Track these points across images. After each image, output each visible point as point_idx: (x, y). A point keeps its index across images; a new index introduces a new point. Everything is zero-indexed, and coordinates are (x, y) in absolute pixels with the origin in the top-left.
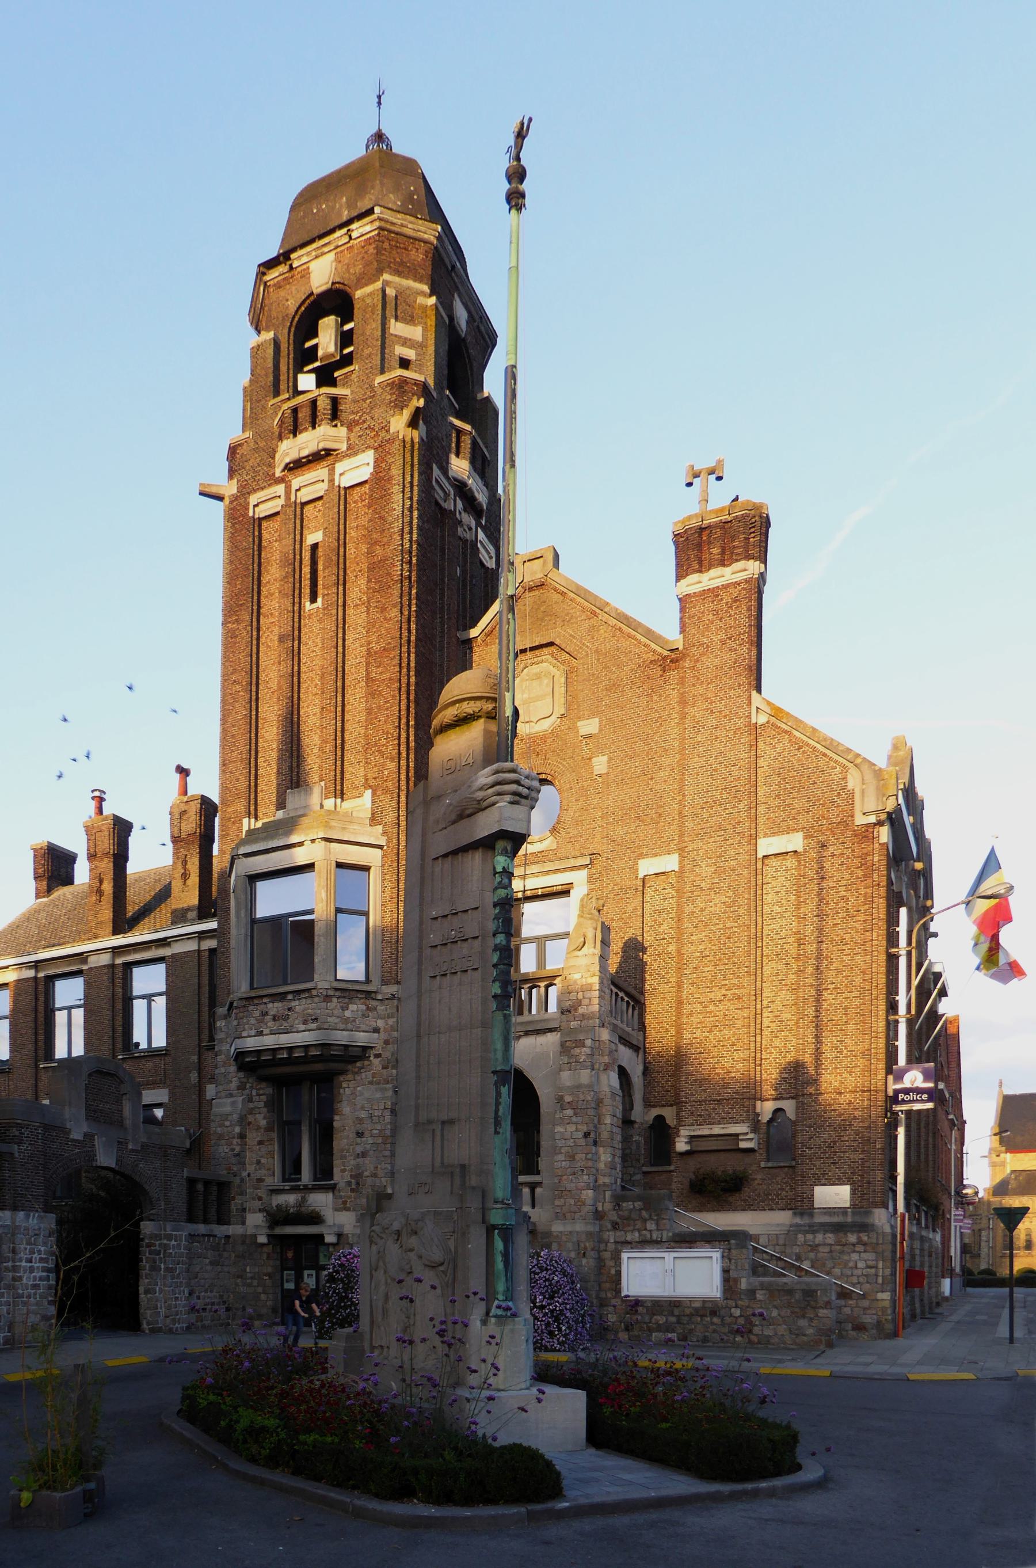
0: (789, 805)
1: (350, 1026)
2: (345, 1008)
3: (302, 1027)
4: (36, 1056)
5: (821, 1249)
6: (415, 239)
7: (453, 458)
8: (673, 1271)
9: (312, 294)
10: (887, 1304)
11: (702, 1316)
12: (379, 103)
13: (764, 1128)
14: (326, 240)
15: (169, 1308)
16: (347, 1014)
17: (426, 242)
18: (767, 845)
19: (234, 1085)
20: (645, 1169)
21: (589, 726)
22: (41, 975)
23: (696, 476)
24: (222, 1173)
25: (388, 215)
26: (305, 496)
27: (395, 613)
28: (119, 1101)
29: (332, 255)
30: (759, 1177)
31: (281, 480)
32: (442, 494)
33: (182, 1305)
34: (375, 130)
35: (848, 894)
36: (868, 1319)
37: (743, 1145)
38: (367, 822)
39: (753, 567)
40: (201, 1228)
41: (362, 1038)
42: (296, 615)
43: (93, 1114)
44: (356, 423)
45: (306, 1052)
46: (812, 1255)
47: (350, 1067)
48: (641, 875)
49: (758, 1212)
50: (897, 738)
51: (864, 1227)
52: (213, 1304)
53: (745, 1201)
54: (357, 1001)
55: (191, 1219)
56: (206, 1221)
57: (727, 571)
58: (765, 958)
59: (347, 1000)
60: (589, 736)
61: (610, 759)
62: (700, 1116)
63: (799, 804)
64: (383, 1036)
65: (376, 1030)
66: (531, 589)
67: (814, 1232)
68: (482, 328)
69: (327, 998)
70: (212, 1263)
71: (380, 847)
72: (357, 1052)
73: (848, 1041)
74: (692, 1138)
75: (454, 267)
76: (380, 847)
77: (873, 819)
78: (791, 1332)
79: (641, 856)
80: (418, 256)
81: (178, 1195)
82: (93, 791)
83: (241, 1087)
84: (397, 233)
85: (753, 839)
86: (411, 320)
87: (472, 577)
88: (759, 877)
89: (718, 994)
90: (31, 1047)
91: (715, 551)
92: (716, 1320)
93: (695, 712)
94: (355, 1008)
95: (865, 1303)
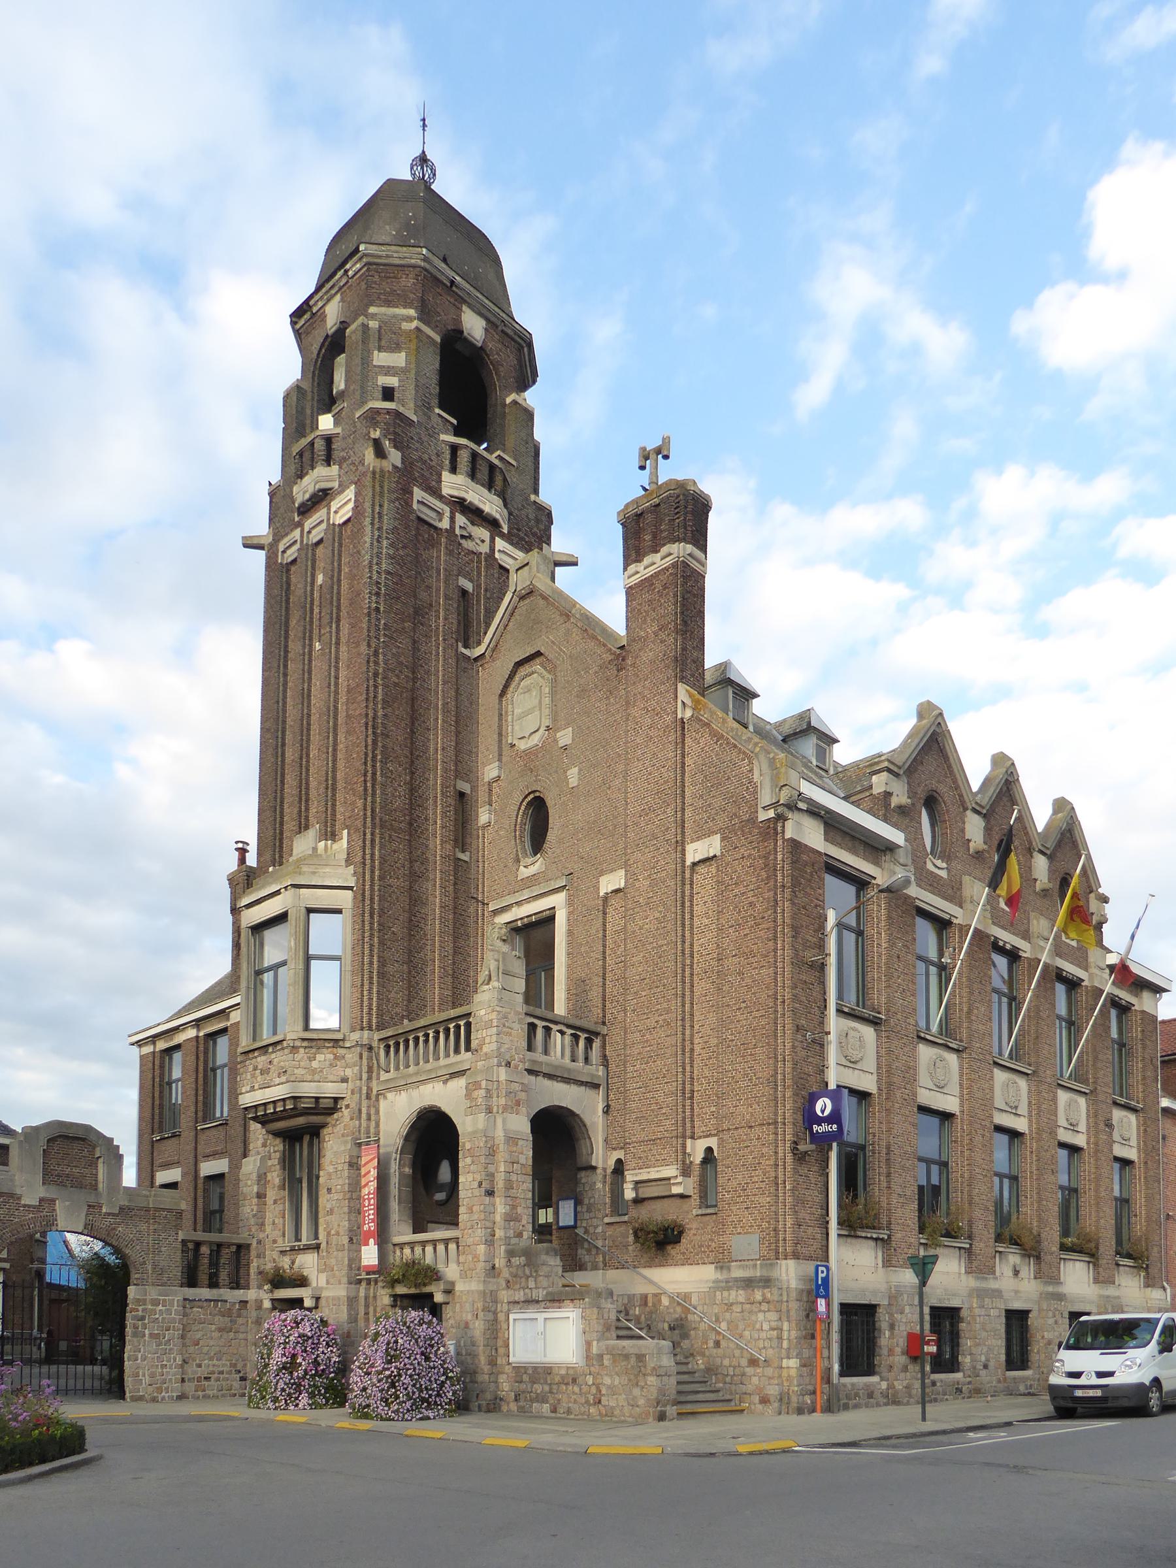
1: (317, 1077)
3: (277, 1081)
4: (196, 1118)
5: (734, 1307)
6: (403, 266)
7: (446, 476)
8: (544, 1333)
9: (327, 336)
10: (793, 1373)
11: (567, 1384)
12: (424, 125)
13: (696, 1171)
14: (331, 283)
15: (152, 1376)
17: (414, 267)
18: (696, 851)
19: (260, 1143)
20: (607, 1220)
21: (565, 737)
22: (201, 1034)
23: (647, 458)
24: (242, 1237)
25: (372, 250)
26: (315, 536)
27: (363, 648)
28: (93, 1163)
30: (694, 1226)
32: (433, 515)
33: (173, 1373)
34: (418, 153)
36: (773, 1391)
37: (676, 1190)
38: (343, 863)
39: (679, 550)
40: (204, 1293)
41: (330, 1089)
42: (307, 657)
43: (48, 1177)
44: (344, 459)
46: (727, 1315)
47: (329, 1119)
48: (601, 894)
49: (694, 1267)
50: (921, 706)
51: (767, 1282)
52: (222, 1373)
53: (684, 1254)
54: (325, 1050)
55: (191, 1280)
56: (213, 1284)
57: (656, 557)
58: (695, 977)
59: (314, 1050)
60: (565, 748)
61: (580, 770)
62: (640, 1158)
63: (718, 802)
64: (351, 1085)
65: (344, 1080)
66: (522, 598)
67: (729, 1289)
68: (509, 332)
69: (294, 1049)
70: (220, 1330)
71: (351, 888)
72: (328, 1104)
73: (757, 1067)
75: (452, 283)
76: (351, 888)
77: (771, 814)
78: (629, 1404)
79: (602, 873)
80: (408, 281)
81: (172, 1260)
82: (237, 842)
83: (264, 1145)
84: (385, 265)
85: (680, 846)
86: (395, 348)
87: (486, 590)
88: (687, 887)
89: (651, 1023)
90: (193, 1109)
91: (648, 537)
92: (576, 1389)
93: (635, 712)
94: (323, 1057)
95: (769, 1371)
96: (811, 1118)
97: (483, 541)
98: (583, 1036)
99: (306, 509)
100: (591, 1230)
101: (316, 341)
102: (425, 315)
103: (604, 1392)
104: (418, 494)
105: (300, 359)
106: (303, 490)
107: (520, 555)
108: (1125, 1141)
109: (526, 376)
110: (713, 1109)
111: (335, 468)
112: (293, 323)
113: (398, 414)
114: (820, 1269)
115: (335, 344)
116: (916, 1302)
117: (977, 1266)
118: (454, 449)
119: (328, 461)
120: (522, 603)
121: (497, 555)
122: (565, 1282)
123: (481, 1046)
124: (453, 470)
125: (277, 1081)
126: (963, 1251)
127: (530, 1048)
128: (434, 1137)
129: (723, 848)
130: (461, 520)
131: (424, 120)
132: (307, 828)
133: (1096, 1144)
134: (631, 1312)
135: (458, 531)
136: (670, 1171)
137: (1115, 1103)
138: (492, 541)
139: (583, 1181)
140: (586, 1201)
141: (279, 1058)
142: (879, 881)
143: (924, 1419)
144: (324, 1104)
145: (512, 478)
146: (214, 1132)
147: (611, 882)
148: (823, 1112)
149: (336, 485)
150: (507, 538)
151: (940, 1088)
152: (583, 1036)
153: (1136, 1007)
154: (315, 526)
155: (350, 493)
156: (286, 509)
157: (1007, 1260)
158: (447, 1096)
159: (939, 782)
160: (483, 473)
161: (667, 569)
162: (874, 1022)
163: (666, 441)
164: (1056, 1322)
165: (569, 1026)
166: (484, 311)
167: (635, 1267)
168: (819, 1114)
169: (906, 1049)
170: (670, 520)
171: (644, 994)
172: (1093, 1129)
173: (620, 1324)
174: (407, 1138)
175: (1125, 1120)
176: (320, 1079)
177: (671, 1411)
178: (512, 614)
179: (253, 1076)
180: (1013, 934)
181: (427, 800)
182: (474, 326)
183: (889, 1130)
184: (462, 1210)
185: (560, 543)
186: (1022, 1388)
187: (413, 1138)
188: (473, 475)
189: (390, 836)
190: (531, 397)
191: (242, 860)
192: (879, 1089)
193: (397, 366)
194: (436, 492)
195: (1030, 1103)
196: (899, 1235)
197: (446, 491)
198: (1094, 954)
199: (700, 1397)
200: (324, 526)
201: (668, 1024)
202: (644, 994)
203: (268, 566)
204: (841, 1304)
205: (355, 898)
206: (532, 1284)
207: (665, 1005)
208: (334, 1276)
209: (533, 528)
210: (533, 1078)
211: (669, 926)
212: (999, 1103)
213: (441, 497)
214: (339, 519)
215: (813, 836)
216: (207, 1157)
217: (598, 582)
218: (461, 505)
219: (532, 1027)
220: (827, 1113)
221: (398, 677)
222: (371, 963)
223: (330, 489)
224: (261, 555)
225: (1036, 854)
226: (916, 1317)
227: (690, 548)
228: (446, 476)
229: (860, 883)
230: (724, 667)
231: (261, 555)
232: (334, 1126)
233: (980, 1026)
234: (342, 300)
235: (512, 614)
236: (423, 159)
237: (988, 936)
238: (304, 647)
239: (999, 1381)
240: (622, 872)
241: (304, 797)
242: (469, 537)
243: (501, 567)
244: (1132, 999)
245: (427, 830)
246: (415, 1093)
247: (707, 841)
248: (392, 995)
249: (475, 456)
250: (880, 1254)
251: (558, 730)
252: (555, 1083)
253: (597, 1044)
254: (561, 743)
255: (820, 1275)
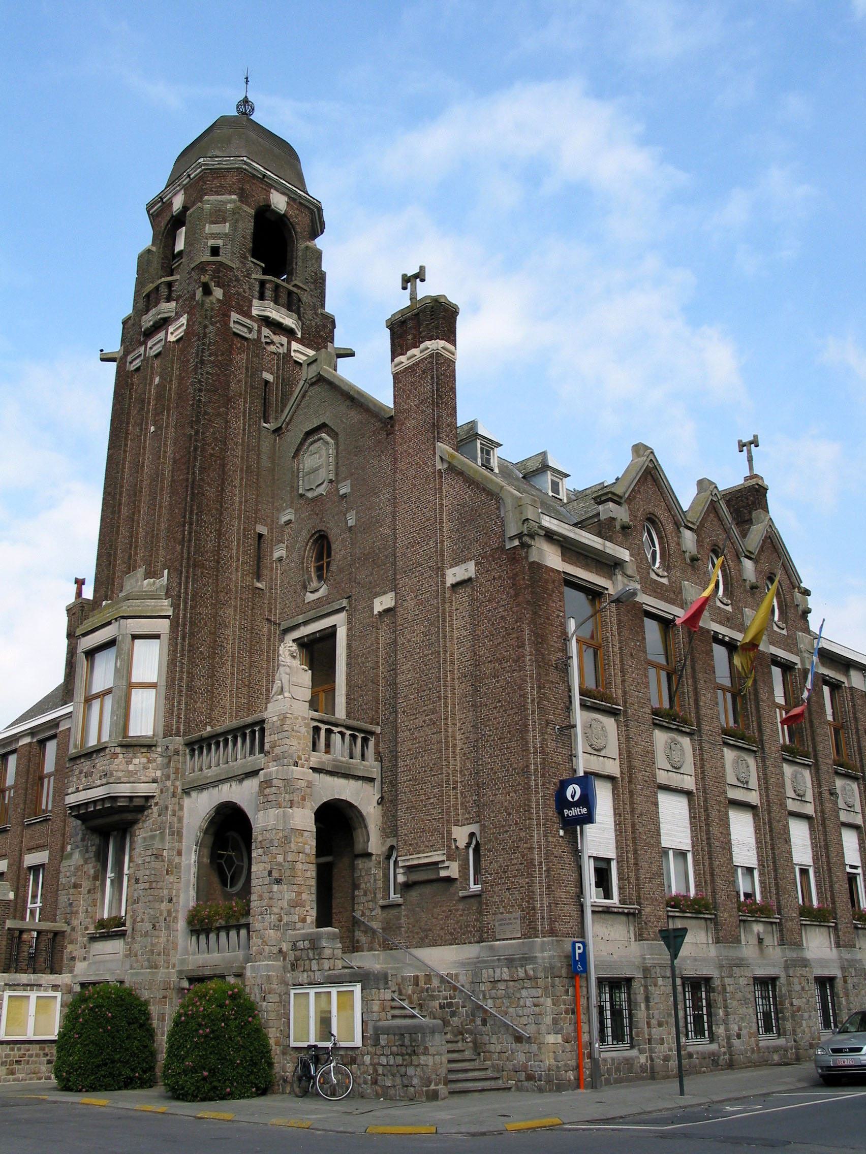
0: (464, 537)
1: (132, 779)
2: (129, 763)
7: (256, 302)
12: (247, 82)
16: (131, 767)
29: (182, 192)
31: (141, 344)
32: (245, 330)
35: (505, 614)
41: (143, 789)
45: (103, 805)
47: (140, 816)
48: (376, 612)
57: (414, 351)
60: (344, 496)
61: (357, 513)
66: (312, 384)
69: (115, 755)
74: (410, 869)
89: (419, 722)
91: (410, 337)
94: (139, 760)
96: (562, 802)
97: (282, 345)
98: (360, 736)
99: (149, 333)
100: (367, 913)
101: (164, 221)
102: (243, 196)
103: (380, 1072)
104: (234, 316)
105: (150, 232)
106: (148, 321)
107: (311, 353)
108: (850, 807)
109: (317, 227)
110: (475, 798)
111: (173, 304)
112: (148, 212)
113: (221, 264)
114: (577, 945)
115: (178, 221)
116: (669, 974)
117: (725, 937)
118: (262, 284)
119: (168, 300)
120: (311, 388)
121: (293, 354)
122: (345, 964)
123: (272, 747)
124: (262, 297)
125: (98, 782)
126: (709, 922)
127: (314, 748)
128: (230, 832)
129: (477, 571)
130: (266, 331)
131: (247, 78)
132: (135, 568)
133: (823, 812)
134: (404, 991)
135: (263, 340)
136: (436, 857)
137: (837, 773)
138: (289, 343)
139: (360, 867)
140: (363, 886)
141: (101, 763)
142: (611, 591)
143: (682, 1093)
144: (137, 802)
145: (305, 298)
146: (38, 827)
147: (382, 603)
148: (573, 797)
149: (173, 314)
150: (301, 341)
151: (676, 768)
152: (360, 736)
153: (846, 685)
154: (154, 345)
155: (184, 320)
156: (135, 333)
157: (752, 931)
158: (241, 794)
159: (655, 506)
160: (284, 298)
161: (426, 359)
162: (613, 713)
163: (422, 268)
164: (803, 989)
165: (348, 728)
166: (287, 191)
167: (407, 947)
168: (570, 799)
169: (644, 736)
170: (425, 323)
171: (412, 697)
172: (819, 797)
173: (394, 1004)
174: (206, 832)
175: (848, 788)
176: (133, 779)
177: (442, 1089)
178: (303, 397)
179: (78, 779)
180: (730, 628)
181: (232, 542)
182: (279, 202)
183: (633, 811)
184: (254, 897)
185: (340, 340)
186: (776, 1057)
187: (211, 831)
188: (276, 302)
189: (202, 573)
190: (320, 242)
191: (79, 593)
192: (622, 772)
193: (223, 231)
194: (247, 314)
195: (759, 777)
196: (648, 910)
197: (255, 312)
198: (803, 640)
199: (470, 1075)
200: (163, 343)
201: (434, 723)
202: (412, 697)
203: (118, 373)
204: (598, 978)
205: (171, 625)
206: (315, 966)
207: (431, 706)
208: (137, 961)
209: (320, 332)
210: (316, 775)
211: (434, 638)
212: (731, 779)
213: (251, 317)
214: (172, 338)
215: (552, 558)
216: (31, 850)
217: (370, 369)
218: (267, 322)
219: (316, 730)
220: (576, 798)
221: (213, 449)
222: (181, 679)
223: (169, 317)
224: (114, 365)
225: (742, 559)
226: (669, 989)
227: (442, 343)
228: (256, 302)
229: (594, 594)
230: (473, 425)
231: (114, 365)
232: (144, 821)
233: (709, 711)
234: (185, 193)
235: (303, 397)
236: (246, 101)
237: (708, 631)
238: (141, 430)
239: (753, 1051)
240: (392, 594)
241: (132, 544)
242: (272, 343)
243: (296, 362)
244: (842, 678)
245: (231, 565)
246: (214, 792)
247: (463, 566)
248: (199, 704)
249: (277, 287)
250: (632, 928)
251: (338, 482)
252: (336, 779)
253: (371, 744)
254: (342, 492)
255: (578, 951)
